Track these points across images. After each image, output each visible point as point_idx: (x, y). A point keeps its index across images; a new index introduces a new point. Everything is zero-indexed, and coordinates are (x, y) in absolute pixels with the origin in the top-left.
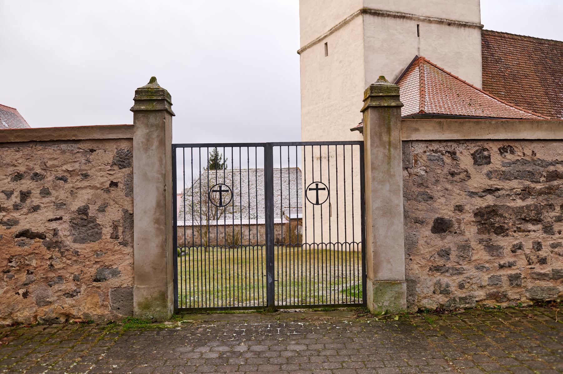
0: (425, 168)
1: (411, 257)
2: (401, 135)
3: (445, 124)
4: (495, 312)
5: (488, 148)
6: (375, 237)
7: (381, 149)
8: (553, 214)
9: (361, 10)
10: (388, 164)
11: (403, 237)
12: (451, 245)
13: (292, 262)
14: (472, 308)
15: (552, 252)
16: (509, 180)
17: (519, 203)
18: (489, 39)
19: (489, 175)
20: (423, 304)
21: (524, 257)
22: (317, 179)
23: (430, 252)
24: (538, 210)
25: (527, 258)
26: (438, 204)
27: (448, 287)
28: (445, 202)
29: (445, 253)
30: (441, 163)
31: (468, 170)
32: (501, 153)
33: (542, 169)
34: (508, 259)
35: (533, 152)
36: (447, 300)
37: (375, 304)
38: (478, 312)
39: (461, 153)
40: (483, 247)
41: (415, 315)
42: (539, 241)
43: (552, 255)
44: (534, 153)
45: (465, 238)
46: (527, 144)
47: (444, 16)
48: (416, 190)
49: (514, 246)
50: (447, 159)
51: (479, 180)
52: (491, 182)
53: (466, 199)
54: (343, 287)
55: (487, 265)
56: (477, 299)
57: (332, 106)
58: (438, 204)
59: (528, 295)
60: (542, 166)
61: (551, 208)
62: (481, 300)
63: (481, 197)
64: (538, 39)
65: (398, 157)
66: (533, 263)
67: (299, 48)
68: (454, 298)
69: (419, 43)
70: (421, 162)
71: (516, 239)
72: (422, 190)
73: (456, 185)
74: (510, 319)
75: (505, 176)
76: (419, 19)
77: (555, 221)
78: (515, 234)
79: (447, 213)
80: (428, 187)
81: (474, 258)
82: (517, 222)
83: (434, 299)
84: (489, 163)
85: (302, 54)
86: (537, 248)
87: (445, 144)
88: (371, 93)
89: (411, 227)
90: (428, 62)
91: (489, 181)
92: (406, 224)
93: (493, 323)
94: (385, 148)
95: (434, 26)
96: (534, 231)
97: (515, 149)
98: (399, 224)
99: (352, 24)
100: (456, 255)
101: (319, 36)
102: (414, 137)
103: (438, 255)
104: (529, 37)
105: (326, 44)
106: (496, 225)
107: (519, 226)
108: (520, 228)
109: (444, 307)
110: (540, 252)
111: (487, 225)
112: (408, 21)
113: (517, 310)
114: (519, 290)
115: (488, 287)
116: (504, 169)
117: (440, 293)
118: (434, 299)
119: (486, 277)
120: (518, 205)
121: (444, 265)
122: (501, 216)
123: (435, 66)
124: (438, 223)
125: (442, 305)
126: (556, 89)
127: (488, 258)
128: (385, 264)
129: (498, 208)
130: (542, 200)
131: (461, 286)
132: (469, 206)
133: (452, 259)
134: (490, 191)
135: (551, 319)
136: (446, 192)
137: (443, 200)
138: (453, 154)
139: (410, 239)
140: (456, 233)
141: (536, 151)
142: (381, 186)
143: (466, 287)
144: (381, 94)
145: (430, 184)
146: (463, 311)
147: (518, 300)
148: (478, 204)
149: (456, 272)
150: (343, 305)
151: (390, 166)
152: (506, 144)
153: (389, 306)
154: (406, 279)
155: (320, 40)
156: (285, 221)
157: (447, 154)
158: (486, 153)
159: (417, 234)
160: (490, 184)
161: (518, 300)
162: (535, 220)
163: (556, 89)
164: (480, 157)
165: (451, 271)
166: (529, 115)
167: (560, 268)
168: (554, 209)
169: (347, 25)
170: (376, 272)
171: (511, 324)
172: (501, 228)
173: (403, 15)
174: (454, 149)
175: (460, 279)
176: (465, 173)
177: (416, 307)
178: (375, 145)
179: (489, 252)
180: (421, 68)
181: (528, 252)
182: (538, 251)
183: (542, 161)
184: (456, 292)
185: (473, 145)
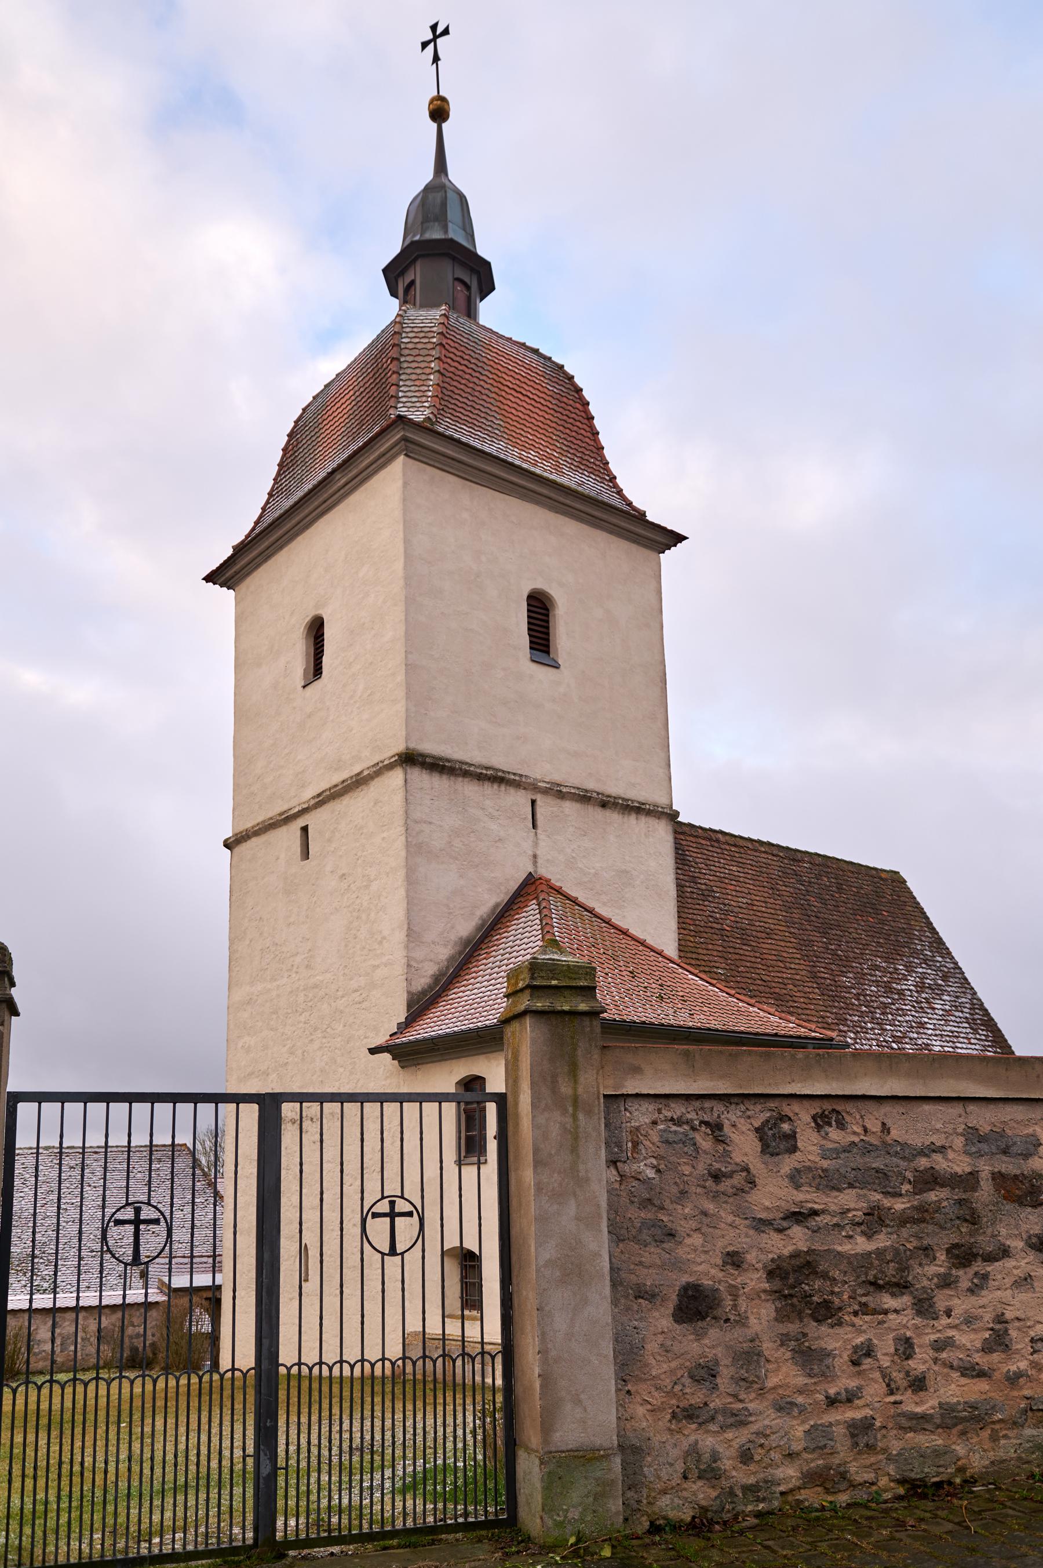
0: (655, 1162)
1: (629, 1387)
2: (600, 1081)
3: (697, 1057)
4: (827, 1519)
5: (791, 1115)
6: (543, 1336)
7: (557, 1115)
8: (932, 1270)
9: (399, 755)
10: (572, 1152)
11: (609, 1335)
12: (719, 1351)
13: (183, 1419)
14: (770, 1513)
15: (936, 1360)
16: (839, 1190)
17: (862, 1245)
18: (698, 849)
19: (795, 1178)
20: (661, 1508)
21: (877, 1375)
22: (392, 1188)
23: (672, 1371)
24: (901, 1259)
25: (884, 1377)
26: (687, 1249)
27: (715, 1461)
28: (703, 1246)
29: (705, 1374)
30: (689, 1150)
31: (751, 1167)
32: (819, 1127)
33: (903, 1164)
34: (844, 1382)
35: (884, 1124)
36: (714, 1494)
37: (545, 1517)
38: (790, 1522)
39: (734, 1126)
40: (789, 1355)
41: (647, 1541)
42: (908, 1334)
43: (936, 1368)
44: (885, 1129)
45: (750, 1333)
46: (870, 1105)
47: (591, 785)
48: (638, 1215)
49: (856, 1349)
50: (705, 1143)
51: (773, 1193)
52: (800, 1196)
53: (747, 1236)
54: (372, 1479)
55: (800, 1400)
56: (782, 1488)
57: (316, 986)
58: (687, 1249)
59: (891, 1469)
60: (904, 1158)
61: (927, 1256)
62: (792, 1491)
63: (780, 1231)
64: (788, 848)
65: (594, 1134)
66: (898, 1389)
68: (731, 1488)
69: (536, 844)
70: (647, 1146)
71: (860, 1331)
72: (650, 1216)
73: (726, 1202)
74: (870, 1535)
75: (828, 1181)
76: (534, 787)
77: (939, 1287)
78: (857, 1321)
79: (707, 1271)
80: (662, 1208)
81: (770, 1383)
82: (860, 1291)
83: (685, 1494)
84: (794, 1149)
85: (236, 850)
86: (904, 1353)
87: (697, 1104)
88: (532, 978)
89: (628, 1309)
90: (559, 891)
91: (795, 1192)
92: (615, 1302)
93: (837, 1548)
94: (564, 1112)
95: (569, 807)
96: (896, 1311)
97: (848, 1118)
98: (600, 1303)
99: (376, 788)
100: (732, 1378)
101: (285, 807)
102: (631, 1087)
103: (691, 1377)
104: (769, 844)
105: (305, 829)
106: (815, 1299)
107: (864, 1299)
108: (865, 1304)
109: (710, 1515)
110: (910, 1362)
111: (795, 1300)
112: (512, 790)
113: (868, 1512)
114: (873, 1460)
115: (805, 1456)
116: (825, 1164)
117: (699, 1478)
118: (685, 1494)
119: (799, 1431)
120: (859, 1250)
121: (706, 1404)
122: (825, 1276)
123: (575, 901)
124: (688, 1297)
125: (704, 1510)
126: (833, 967)
127: (801, 1380)
128: (568, 1407)
129: (818, 1258)
130: (908, 1238)
131: (745, 1457)
132: (754, 1254)
133: (722, 1388)
134: (798, 1217)
135: (957, 1527)
136: (704, 1219)
137: (697, 1240)
138: (716, 1128)
139: (627, 1339)
140: (727, 1320)
141: (889, 1123)
142: (555, 1207)
143: (757, 1458)
144: (554, 982)
145: (668, 1201)
146: (756, 1521)
147: (873, 1484)
148: (775, 1250)
149: (731, 1420)
150: (456, 1528)
151: (578, 1156)
152: (828, 1106)
153: (582, 1520)
154: (619, 1445)
155: (287, 819)
156: (155, 1296)
157: (703, 1128)
158: (786, 1127)
159: (641, 1325)
160: (798, 1199)
161: (873, 1484)
162: (897, 1285)
163: (833, 967)
164: (774, 1135)
165: (720, 1418)
166: (789, 1027)
167: (955, 1400)
168: (935, 1259)
170: (547, 1429)
171: (877, 1545)
172: (826, 1304)
173: (500, 774)
174: (719, 1117)
175: (740, 1437)
176: (744, 1174)
177: (644, 1518)
178: (543, 1105)
179: (803, 1366)
180: (544, 904)
181: (886, 1362)
182: (907, 1359)
183: (904, 1145)
184: (734, 1473)
185: (759, 1107)
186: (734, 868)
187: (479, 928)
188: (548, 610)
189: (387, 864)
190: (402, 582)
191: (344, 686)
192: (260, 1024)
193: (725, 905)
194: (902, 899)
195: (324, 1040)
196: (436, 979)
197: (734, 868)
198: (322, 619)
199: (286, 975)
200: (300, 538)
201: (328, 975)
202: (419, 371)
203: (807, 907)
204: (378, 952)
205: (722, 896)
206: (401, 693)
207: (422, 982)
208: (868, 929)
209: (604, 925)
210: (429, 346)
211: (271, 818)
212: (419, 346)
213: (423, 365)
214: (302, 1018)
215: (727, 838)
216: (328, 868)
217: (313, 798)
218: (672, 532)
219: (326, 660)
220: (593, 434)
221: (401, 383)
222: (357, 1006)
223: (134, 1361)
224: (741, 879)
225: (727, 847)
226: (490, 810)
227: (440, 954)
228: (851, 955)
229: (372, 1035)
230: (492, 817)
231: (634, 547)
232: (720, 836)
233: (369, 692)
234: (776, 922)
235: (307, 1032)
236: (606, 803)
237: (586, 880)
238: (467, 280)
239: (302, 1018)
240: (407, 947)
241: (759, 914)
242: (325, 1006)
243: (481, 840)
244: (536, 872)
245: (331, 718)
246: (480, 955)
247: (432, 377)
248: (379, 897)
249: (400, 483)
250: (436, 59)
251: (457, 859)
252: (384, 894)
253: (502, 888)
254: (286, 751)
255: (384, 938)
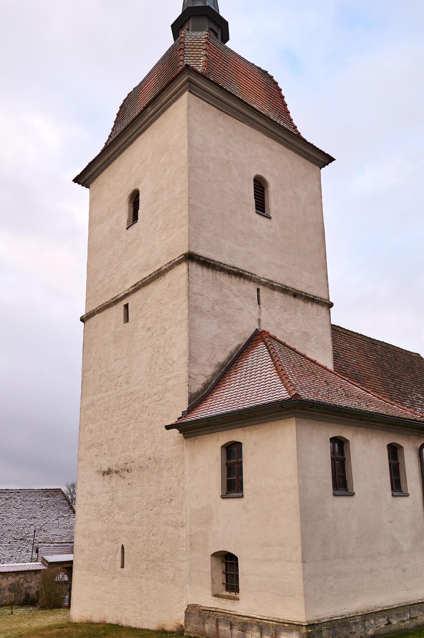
9: (185, 255)
57: (131, 393)
64: (370, 338)
67: (83, 313)
69: (260, 313)
85: (87, 322)
95: (277, 295)
112: (247, 282)
155: (116, 301)
169: (162, 277)
173: (241, 271)
186: (348, 345)
187: (229, 358)
188: (264, 189)
189: (176, 319)
190: (186, 160)
191: (151, 223)
192: (98, 417)
193: (346, 362)
195: (136, 424)
196: (206, 386)
197: (348, 345)
199: (114, 388)
201: (139, 386)
202: (194, 55)
203: (383, 367)
204: (170, 370)
205: (344, 357)
206: (186, 221)
207: (197, 387)
208: (412, 379)
209: (302, 357)
210: (200, 44)
211: (107, 302)
212: (195, 44)
213: (197, 53)
214: (123, 412)
215: (342, 330)
216: (140, 326)
217: (132, 287)
218: (327, 155)
219: (140, 212)
220: (284, 105)
221: (185, 61)
222: (156, 403)
223: (27, 601)
224: (352, 350)
225: (343, 334)
226: (235, 292)
227: (206, 371)
228: (407, 391)
229: (166, 420)
230: (236, 296)
231: (307, 162)
232: (339, 329)
233: (166, 224)
234: (370, 372)
235: (126, 420)
236: (297, 295)
237: (286, 336)
238: (216, 31)
239: (123, 412)
240: (188, 366)
241: (362, 368)
242: (137, 404)
243: (230, 308)
244: (260, 328)
245: (143, 242)
246: (231, 373)
247: (202, 58)
248: (171, 338)
249: (186, 106)
251: (217, 317)
252: (174, 336)
253: (242, 336)
254: (117, 265)
255: (174, 362)
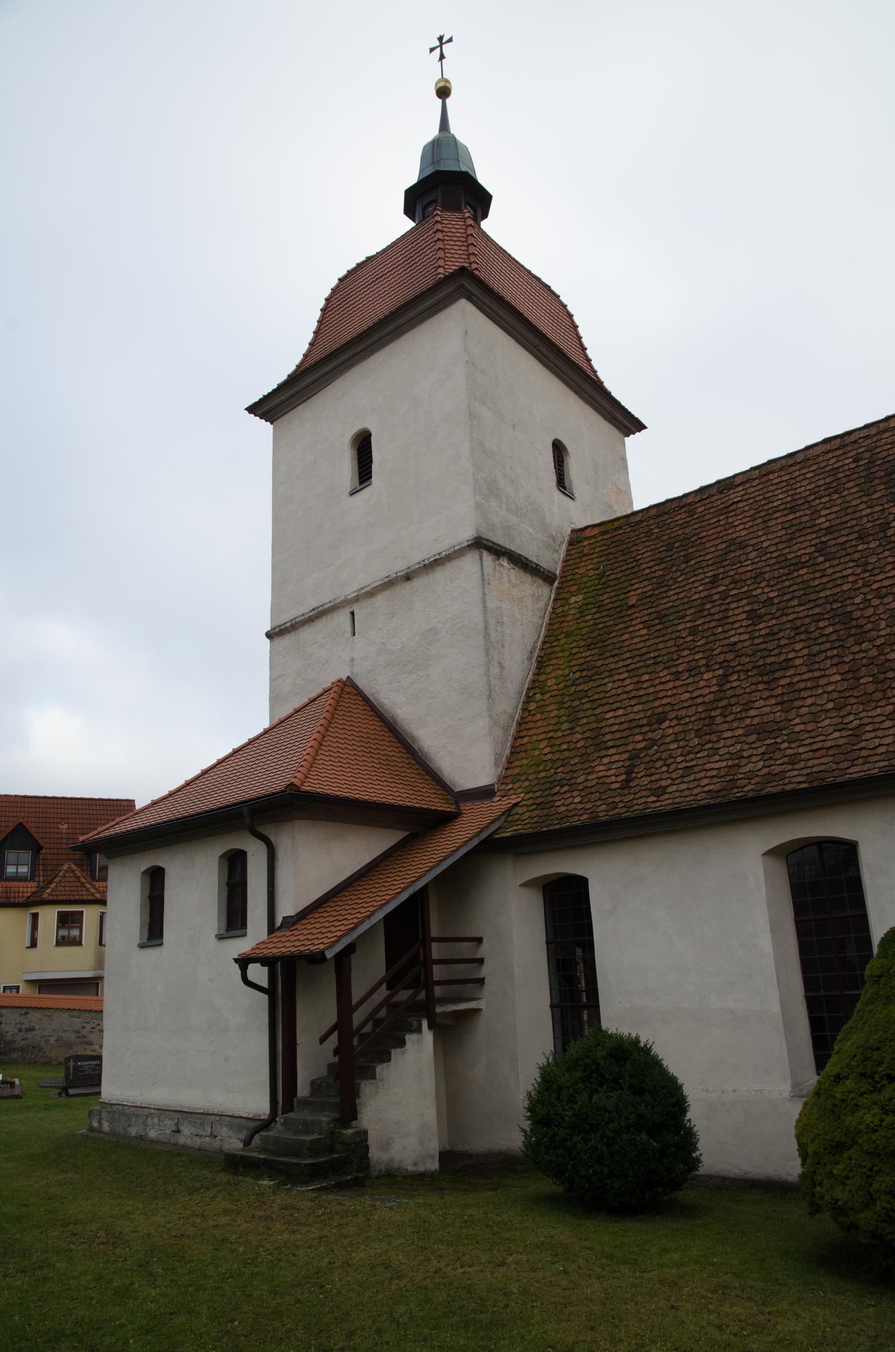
105: (352, 613)
194: (566, 654)
198: (370, 435)
200: (408, 336)
250: (442, 57)
